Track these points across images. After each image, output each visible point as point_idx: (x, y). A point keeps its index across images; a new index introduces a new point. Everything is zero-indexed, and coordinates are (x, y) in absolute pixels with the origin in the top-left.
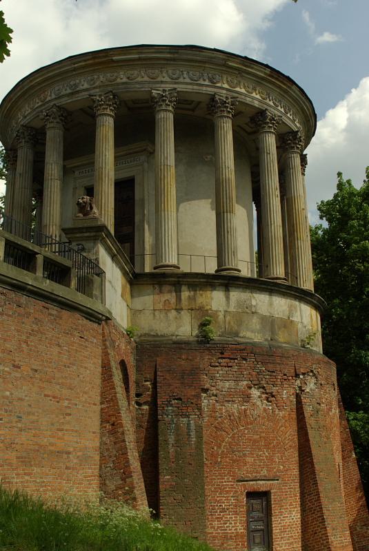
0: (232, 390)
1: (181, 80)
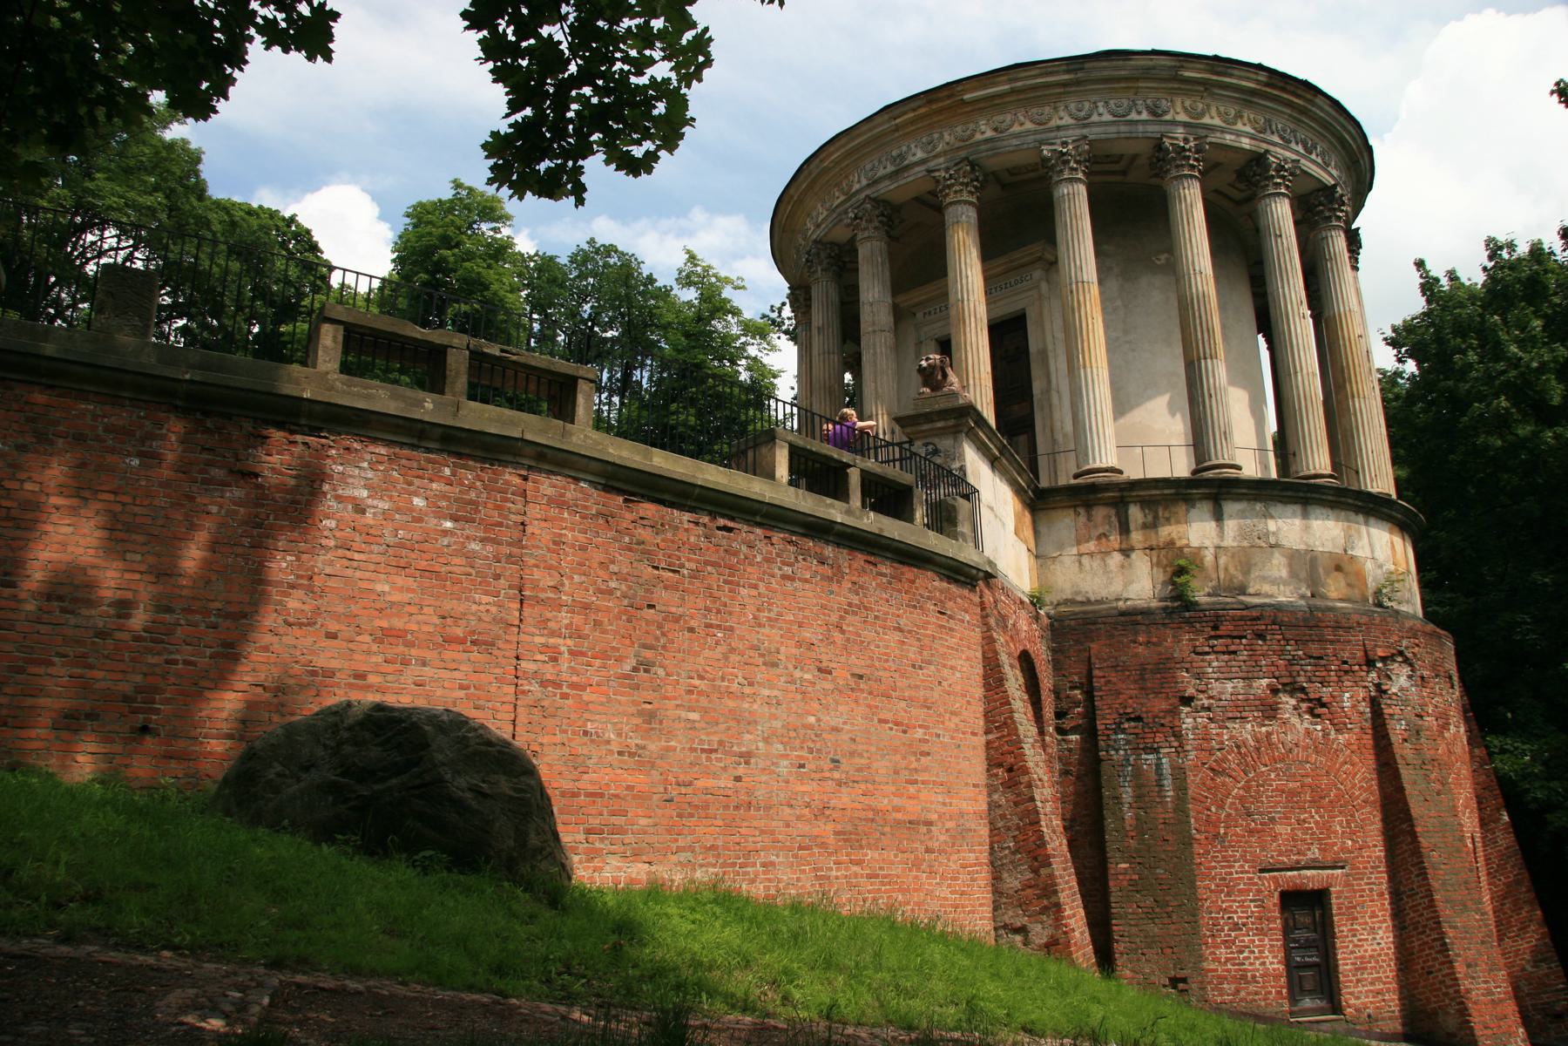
0: (1240, 697)
1: (1095, 118)
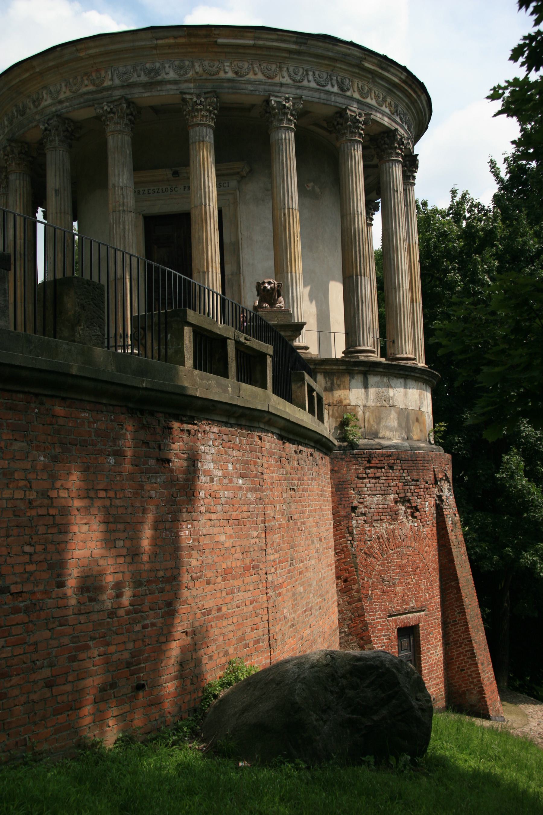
0: (381, 506)
1: (305, 83)
